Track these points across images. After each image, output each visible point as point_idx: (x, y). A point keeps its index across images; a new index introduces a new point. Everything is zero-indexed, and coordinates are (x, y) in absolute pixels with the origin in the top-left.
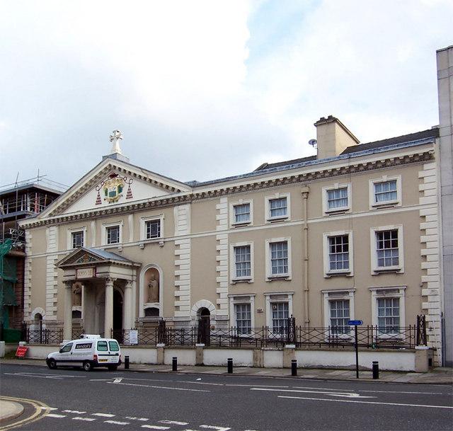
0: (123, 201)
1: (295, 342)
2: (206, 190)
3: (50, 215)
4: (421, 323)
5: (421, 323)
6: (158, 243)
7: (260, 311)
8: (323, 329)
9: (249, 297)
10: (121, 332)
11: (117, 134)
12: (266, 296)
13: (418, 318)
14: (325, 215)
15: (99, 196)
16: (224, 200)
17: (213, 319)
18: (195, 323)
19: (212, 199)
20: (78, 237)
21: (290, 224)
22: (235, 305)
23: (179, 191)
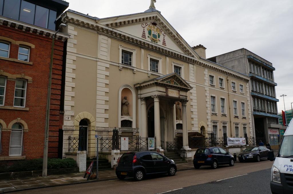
3: (107, 25)
6: (133, 70)
9: (238, 124)
12: (221, 122)
14: (219, 88)
17: (93, 130)
19: (202, 67)
20: (178, 69)
21: (224, 91)
23: (193, 56)
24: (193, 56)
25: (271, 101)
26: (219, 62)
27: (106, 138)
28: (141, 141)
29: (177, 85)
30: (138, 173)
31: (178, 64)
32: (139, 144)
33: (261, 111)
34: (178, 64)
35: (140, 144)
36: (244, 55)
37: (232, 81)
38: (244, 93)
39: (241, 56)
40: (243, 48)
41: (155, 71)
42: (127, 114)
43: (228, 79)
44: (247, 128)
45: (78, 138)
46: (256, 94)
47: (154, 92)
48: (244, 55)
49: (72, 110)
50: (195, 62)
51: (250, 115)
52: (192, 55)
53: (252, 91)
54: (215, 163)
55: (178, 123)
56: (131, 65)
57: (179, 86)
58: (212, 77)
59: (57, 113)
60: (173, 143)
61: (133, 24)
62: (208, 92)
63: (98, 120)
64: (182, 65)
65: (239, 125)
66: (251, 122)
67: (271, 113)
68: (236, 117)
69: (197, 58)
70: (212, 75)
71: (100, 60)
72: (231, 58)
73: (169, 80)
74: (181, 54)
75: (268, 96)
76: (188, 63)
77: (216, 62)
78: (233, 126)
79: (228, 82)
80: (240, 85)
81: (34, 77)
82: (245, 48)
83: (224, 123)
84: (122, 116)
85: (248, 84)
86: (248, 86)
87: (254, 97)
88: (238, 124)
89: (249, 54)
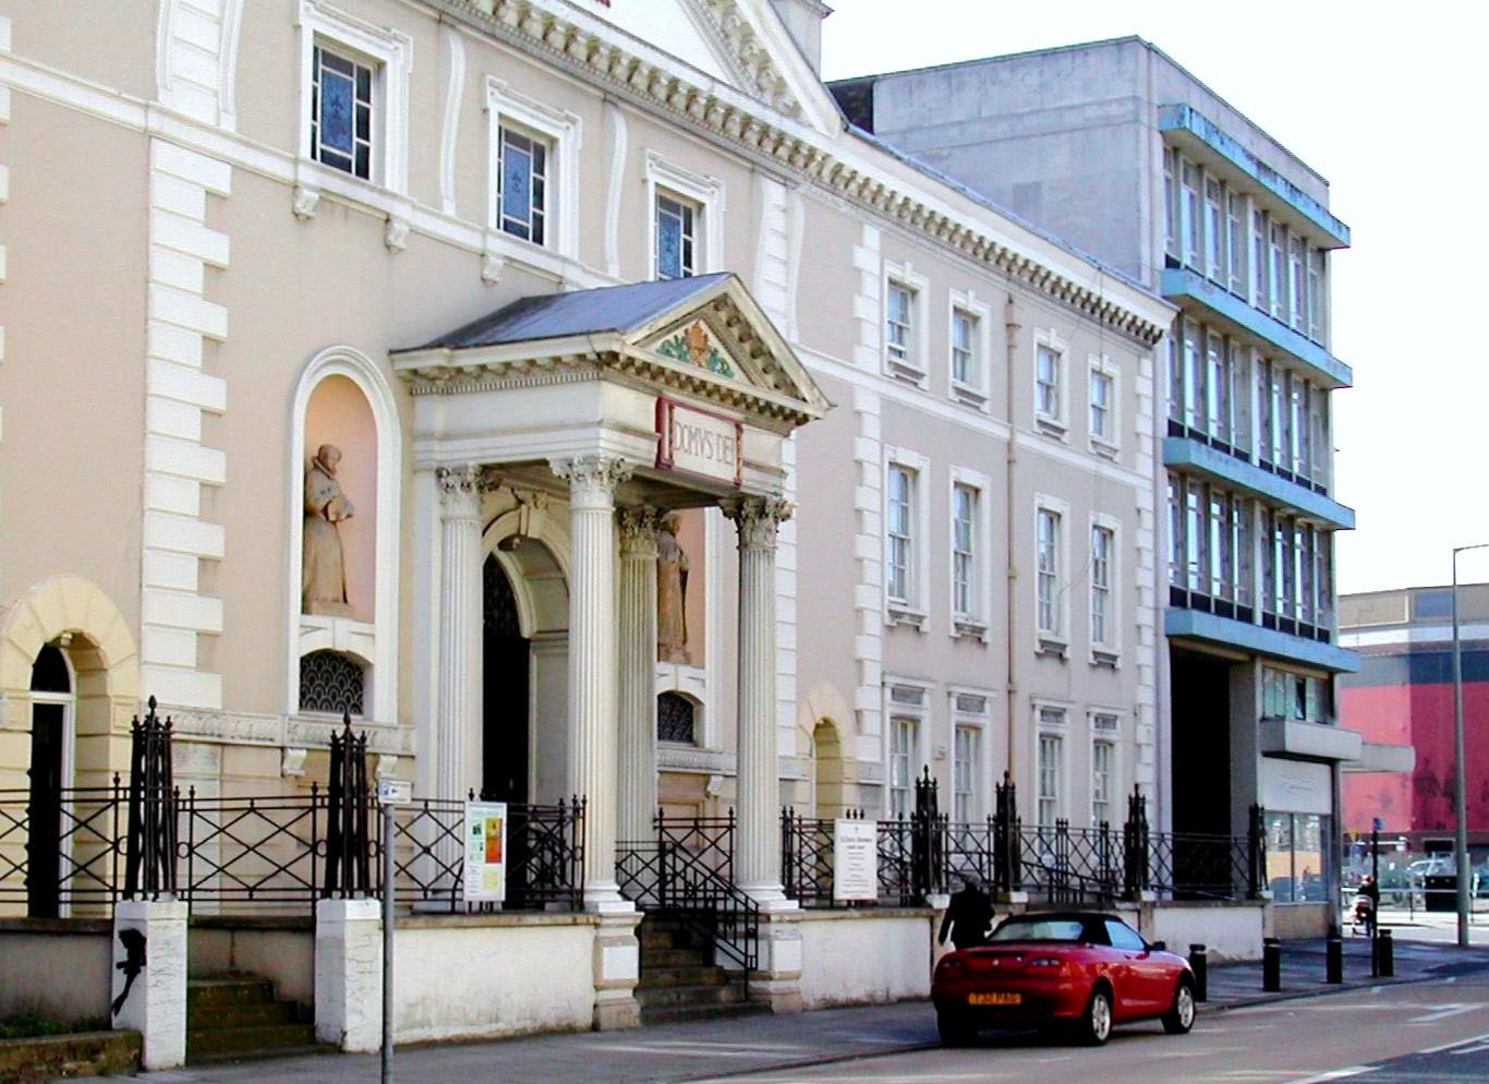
23: (794, 111)
25: (1281, 517)
26: (903, 132)
27: (247, 804)
29: (726, 372)
33: (1224, 610)
36: (1135, 99)
37: (1039, 336)
38: (1117, 444)
39: (1114, 110)
40: (1136, 39)
41: (344, 165)
42: (336, 601)
43: (1018, 317)
44: (1119, 747)
45: (27, 796)
46: (1201, 457)
47: (557, 435)
48: (1135, 99)
49: (205, 589)
50: (800, 161)
51: (1148, 636)
52: (787, 100)
53: (1175, 429)
54: (1100, 1005)
55: (317, 643)
56: (1134, 468)
57: (737, 383)
58: (904, 293)
60: (648, 857)
62: (872, 427)
63: (155, 646)
64: (713, 184)
65: (1067, 716)
66: (1146, 696)
67: (1287, 626)
68: (1054, 651)
69: (820, 127)
70: (911, 278)
71: (183, 133)
72: (1019, 116)
73: (680, 333)
74: (723, 94)
75: (1216, 445)
76: (754, 168)
77: (870, 129)
78: (1031, 728)
79: (1010, 347)
80: (1097, 373)
82: (1147, 38)
83: (964, 703)
84: (310, 620)
85: (1147, 365)
86: (1144, 387)
87: (1182, 476)
88: (1058, 714)
89: (1178, 93)
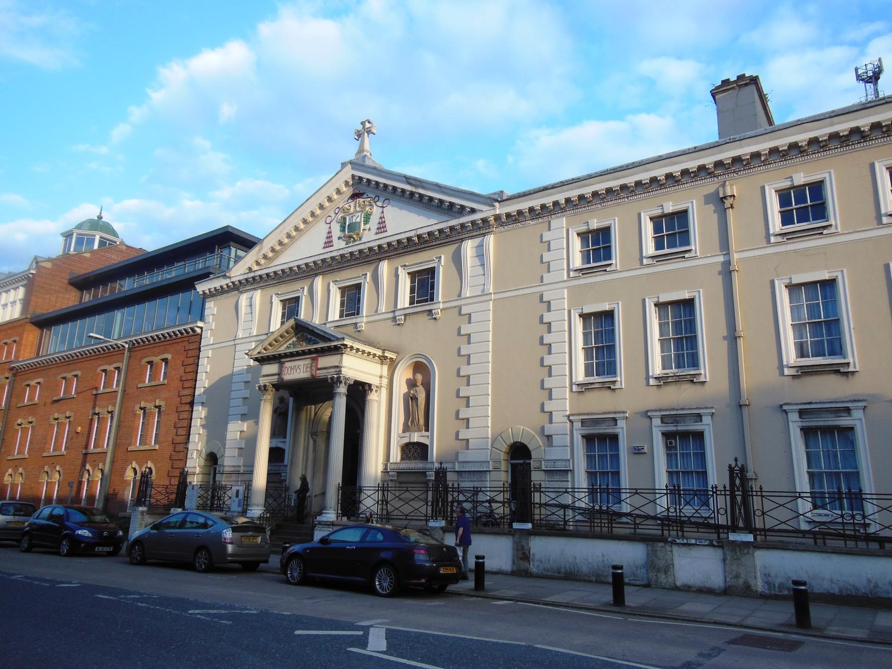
0: (369, 238)
1: (749, 528)
2: (524, 205)
4: (738, 482)
5: (738, 482)
7: (637, 451)
8: (653, 491)
10: (354, 493)
11: (368, 125)
13: (731, 470)
15: (329, 232)
16: (560, 223)
17: (539, 469)
18: (503, 477)
19: (535, 222)
20: (291, 306)
22: (664, 434)
23: (473, 211)
24: (473, 211)
28: (154, 492)
30: (200, 554)
31: (421, 263)
32: (380, 502)
34: (421, 263)
35: (378, 501)
55: (406, 440)
59: (180, 448)
61: (403, 199)
81: (166, 399)
